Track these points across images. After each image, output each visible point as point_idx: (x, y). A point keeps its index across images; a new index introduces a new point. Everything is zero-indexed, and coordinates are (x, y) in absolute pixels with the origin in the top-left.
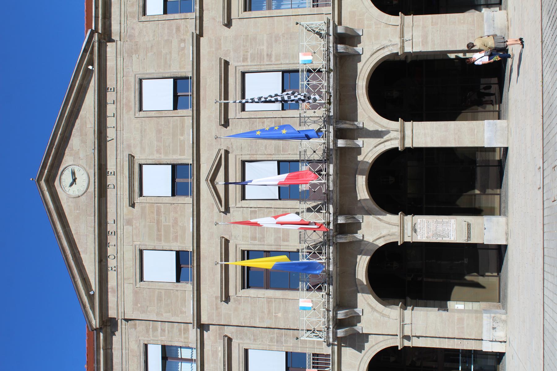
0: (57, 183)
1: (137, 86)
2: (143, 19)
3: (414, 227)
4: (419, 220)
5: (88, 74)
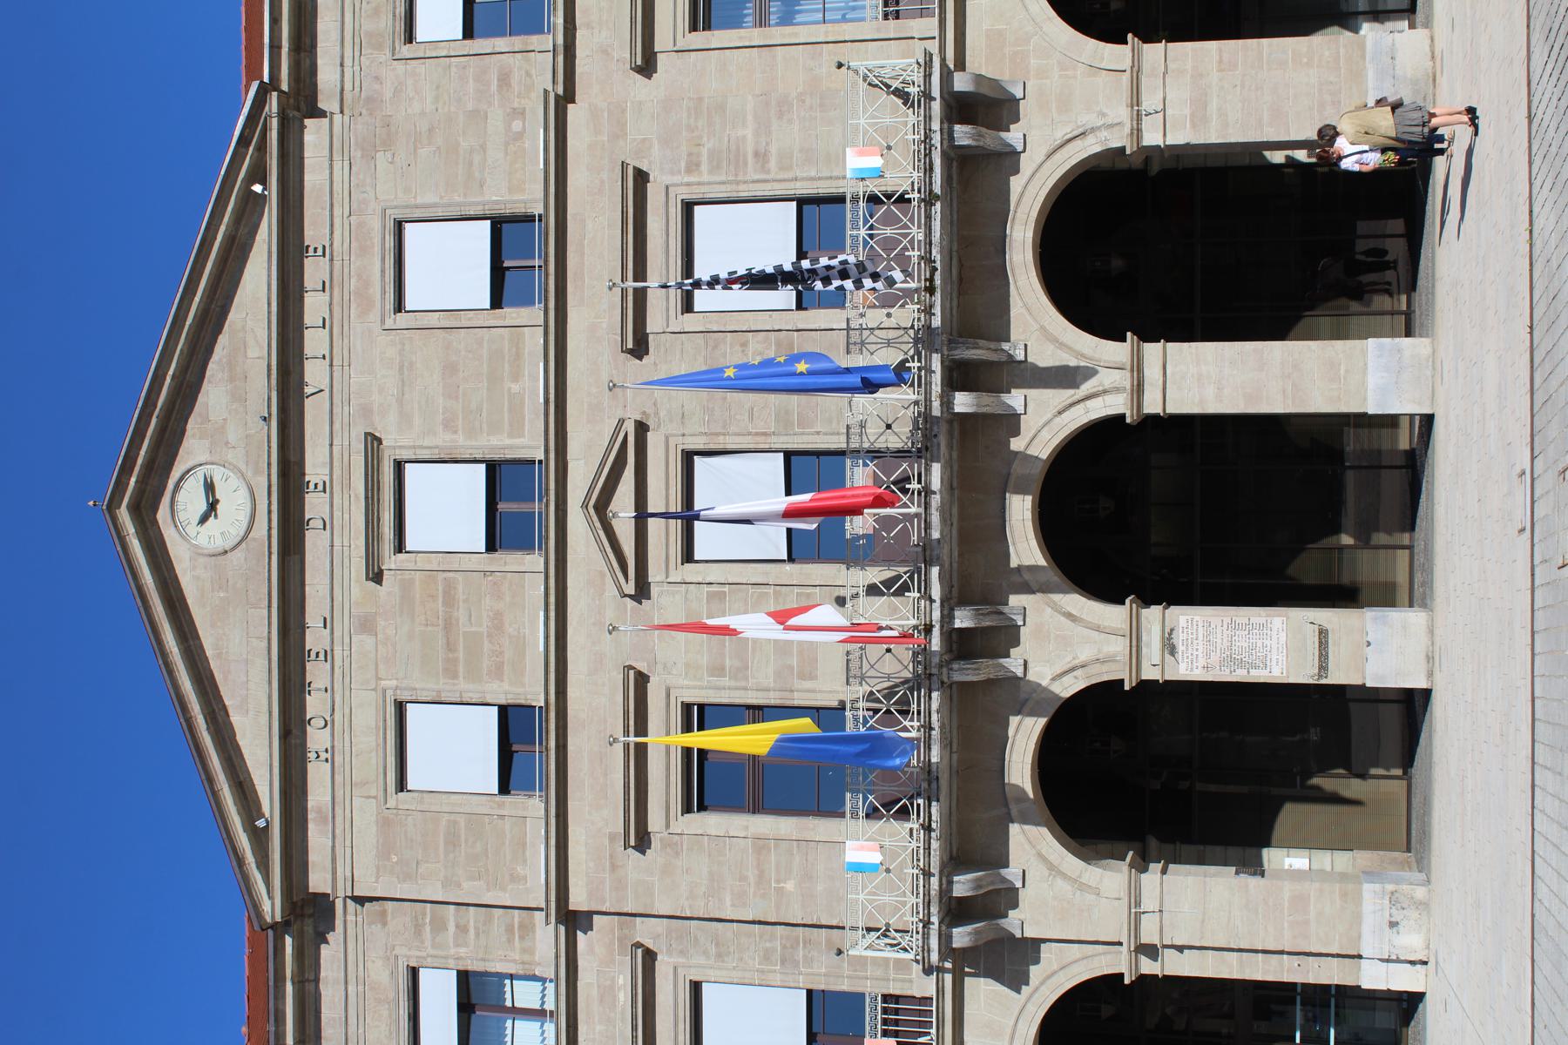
0: (163, 514)
1: (390, 242)
2: (406, 50)
3: (1170, 639)
4: (1183, 620)
5: (251, 207)
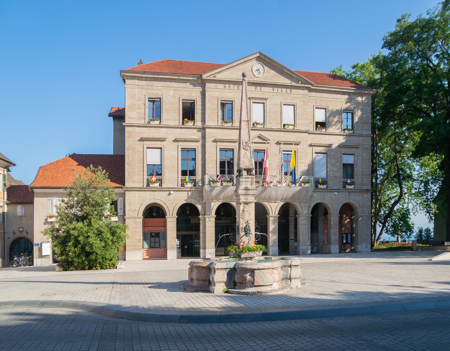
2: (315, 107)
